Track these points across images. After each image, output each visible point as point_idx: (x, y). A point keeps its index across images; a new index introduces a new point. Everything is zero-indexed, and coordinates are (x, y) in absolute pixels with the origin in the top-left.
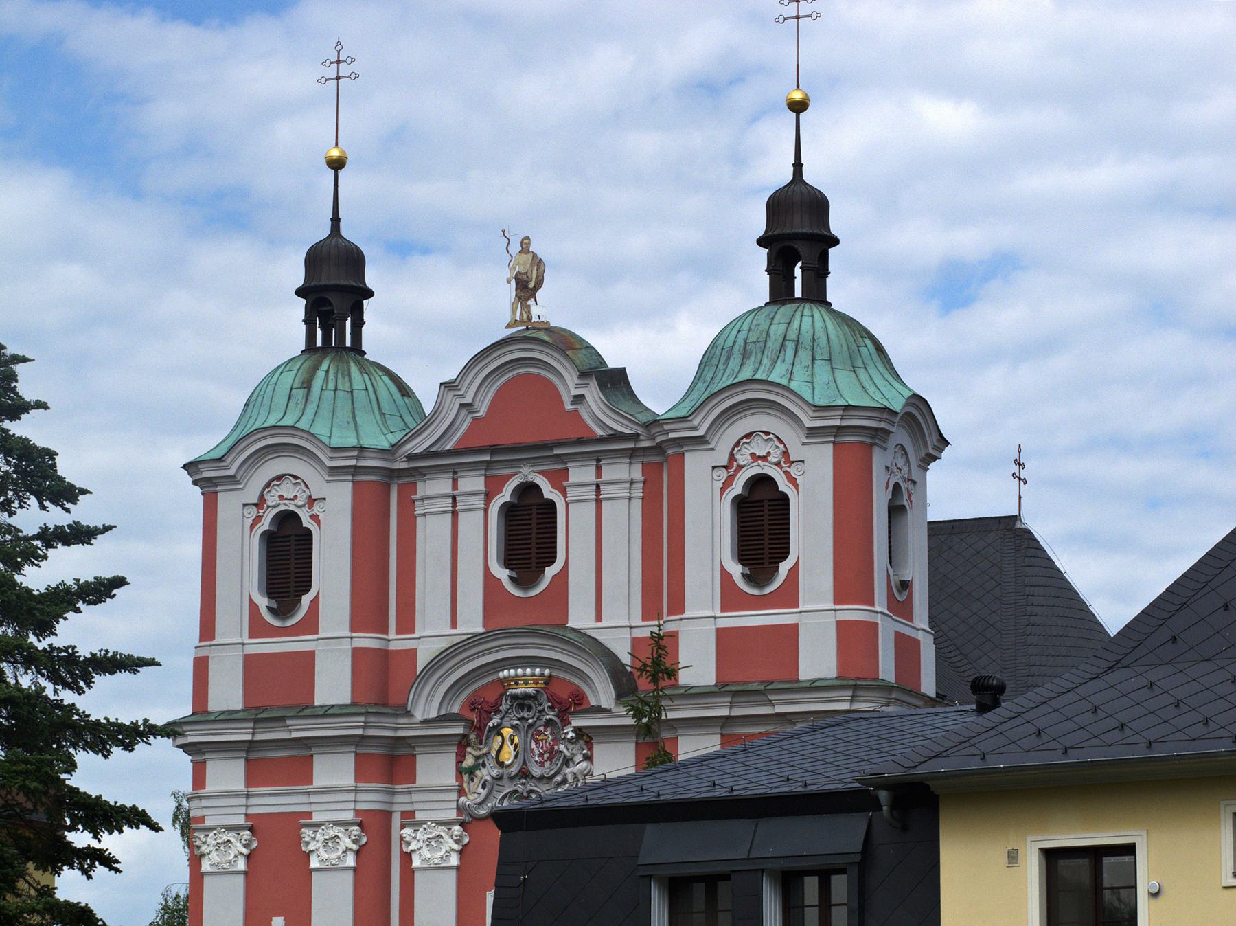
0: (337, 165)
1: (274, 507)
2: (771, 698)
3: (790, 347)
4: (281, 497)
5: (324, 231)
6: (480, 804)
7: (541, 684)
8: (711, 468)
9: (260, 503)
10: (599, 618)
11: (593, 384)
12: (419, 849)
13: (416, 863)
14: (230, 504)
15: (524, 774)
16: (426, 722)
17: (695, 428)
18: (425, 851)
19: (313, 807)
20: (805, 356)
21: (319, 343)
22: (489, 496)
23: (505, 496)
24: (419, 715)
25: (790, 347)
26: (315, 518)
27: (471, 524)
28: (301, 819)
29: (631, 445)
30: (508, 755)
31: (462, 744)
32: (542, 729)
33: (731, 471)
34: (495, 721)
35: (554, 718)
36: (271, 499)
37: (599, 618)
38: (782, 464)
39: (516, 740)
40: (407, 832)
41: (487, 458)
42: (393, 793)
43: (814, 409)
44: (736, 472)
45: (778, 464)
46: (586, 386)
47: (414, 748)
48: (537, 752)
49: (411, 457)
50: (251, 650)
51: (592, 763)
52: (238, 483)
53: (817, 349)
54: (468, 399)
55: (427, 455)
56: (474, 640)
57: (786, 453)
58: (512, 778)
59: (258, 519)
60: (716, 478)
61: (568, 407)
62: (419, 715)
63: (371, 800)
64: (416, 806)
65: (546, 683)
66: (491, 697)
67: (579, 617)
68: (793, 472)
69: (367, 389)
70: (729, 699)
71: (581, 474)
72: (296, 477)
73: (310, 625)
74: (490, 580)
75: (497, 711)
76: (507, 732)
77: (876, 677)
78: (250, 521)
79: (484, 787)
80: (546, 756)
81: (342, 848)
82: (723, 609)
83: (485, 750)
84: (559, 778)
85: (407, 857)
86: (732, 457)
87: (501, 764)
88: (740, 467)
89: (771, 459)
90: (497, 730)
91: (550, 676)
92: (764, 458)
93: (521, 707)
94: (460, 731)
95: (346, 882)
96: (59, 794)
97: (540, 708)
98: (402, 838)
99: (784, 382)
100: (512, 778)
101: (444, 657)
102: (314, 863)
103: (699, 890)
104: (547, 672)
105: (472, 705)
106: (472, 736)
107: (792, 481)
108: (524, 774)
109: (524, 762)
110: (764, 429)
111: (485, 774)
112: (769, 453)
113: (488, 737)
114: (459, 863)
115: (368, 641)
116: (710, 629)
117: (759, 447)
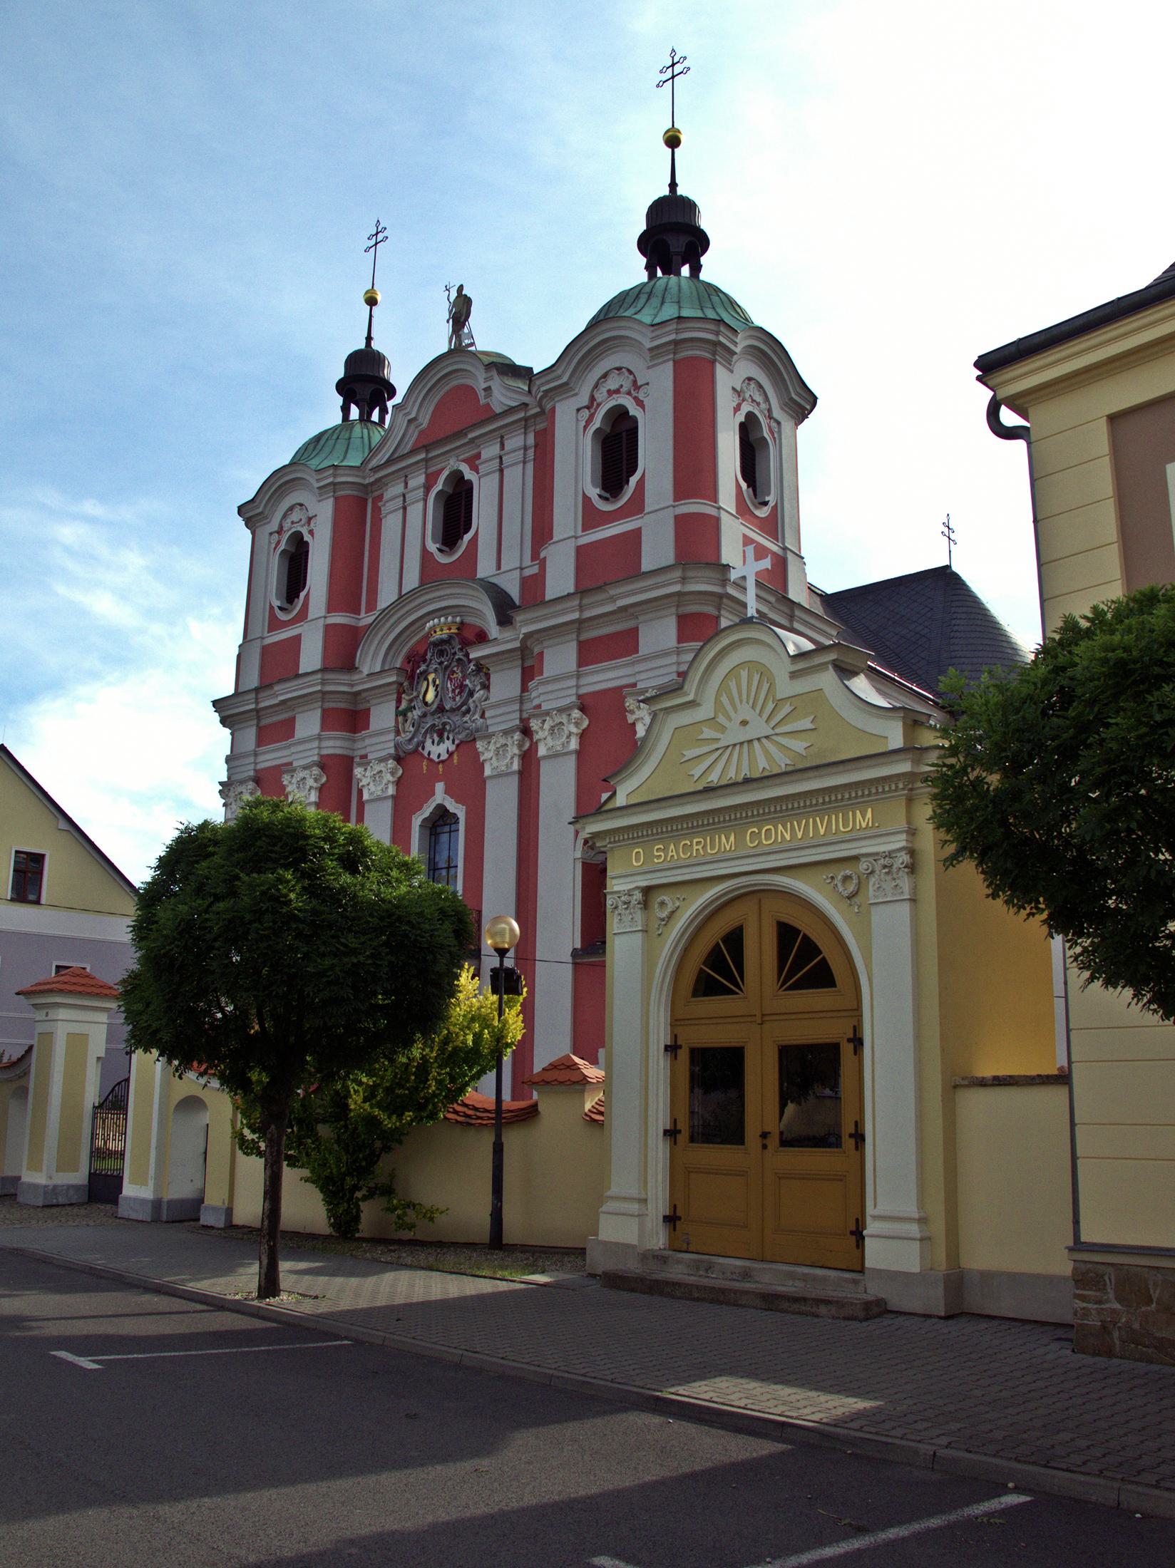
2: (612, 592)
4: (293, 523)
6: (410, 740)
7: (454, 630)
8: (575, 411)
9: (279, 532)
11: (494, 373)
12: (368, 785)
13: (366, 796)
17: (559, 377)
18: (372, 787)
19: (294, 757)
22: (427, 488)
28: (288, 768)
29: (522, 415)
30: (430, 697)
32: (455, 669)
33: (592, 411)
34: (423, 667)
35: (462, 657)
36: (287, 525)
37: (499, 567)
38: (632, 392)
39: (437, 682)
41: (423, 456)
42: (354, 741)
43: (652, 328)
46: (491, 378)
47: (368, 701)
48: (450, 689)
49: (376, 469)
51: (489, 691)
52: (266, 518)
54: (413, 416)
55: (390, 462)
57: (635, 382)
58: (433, 714)
60: (580, 419)
62: (366, 670)
63: (334, 745)
64: (368, 749)
65: (458, 629)
67: (485, 568)
69: (362, 437)
70: (577, 602)
72: (301, 505)
73: (636, 506)
74: (425, 553)
75: (425, 661)
78: (273, 545)
79: (413, 726)
80: (457, 691)
81: (385, 781)
83: (415, 694)
85: (360, 792)
86: (592, 398)
87: (426, 704)
88: (599, 405)
89: (624, 389)
90: (425, 675)
91: (462, 623)
92: (617, 391)
93: (441, 653)
94: (393, 679)
95: (570, 764)
96: (1165, 659)
97: (453, 651)
100: (433, 714)
101: (382, 618)
102: (488, 771)
103: (746, 744)
104: (458, 619)
106: (406, 684)
107: (640, 403)
108: (441, 709)
109: (441, 700)
110: (630, 368)
111: (417, 713)
112: (622, 386)
113: (418, 683)
114: (395, 793)
115: (338, 619)
117: (612, 384)
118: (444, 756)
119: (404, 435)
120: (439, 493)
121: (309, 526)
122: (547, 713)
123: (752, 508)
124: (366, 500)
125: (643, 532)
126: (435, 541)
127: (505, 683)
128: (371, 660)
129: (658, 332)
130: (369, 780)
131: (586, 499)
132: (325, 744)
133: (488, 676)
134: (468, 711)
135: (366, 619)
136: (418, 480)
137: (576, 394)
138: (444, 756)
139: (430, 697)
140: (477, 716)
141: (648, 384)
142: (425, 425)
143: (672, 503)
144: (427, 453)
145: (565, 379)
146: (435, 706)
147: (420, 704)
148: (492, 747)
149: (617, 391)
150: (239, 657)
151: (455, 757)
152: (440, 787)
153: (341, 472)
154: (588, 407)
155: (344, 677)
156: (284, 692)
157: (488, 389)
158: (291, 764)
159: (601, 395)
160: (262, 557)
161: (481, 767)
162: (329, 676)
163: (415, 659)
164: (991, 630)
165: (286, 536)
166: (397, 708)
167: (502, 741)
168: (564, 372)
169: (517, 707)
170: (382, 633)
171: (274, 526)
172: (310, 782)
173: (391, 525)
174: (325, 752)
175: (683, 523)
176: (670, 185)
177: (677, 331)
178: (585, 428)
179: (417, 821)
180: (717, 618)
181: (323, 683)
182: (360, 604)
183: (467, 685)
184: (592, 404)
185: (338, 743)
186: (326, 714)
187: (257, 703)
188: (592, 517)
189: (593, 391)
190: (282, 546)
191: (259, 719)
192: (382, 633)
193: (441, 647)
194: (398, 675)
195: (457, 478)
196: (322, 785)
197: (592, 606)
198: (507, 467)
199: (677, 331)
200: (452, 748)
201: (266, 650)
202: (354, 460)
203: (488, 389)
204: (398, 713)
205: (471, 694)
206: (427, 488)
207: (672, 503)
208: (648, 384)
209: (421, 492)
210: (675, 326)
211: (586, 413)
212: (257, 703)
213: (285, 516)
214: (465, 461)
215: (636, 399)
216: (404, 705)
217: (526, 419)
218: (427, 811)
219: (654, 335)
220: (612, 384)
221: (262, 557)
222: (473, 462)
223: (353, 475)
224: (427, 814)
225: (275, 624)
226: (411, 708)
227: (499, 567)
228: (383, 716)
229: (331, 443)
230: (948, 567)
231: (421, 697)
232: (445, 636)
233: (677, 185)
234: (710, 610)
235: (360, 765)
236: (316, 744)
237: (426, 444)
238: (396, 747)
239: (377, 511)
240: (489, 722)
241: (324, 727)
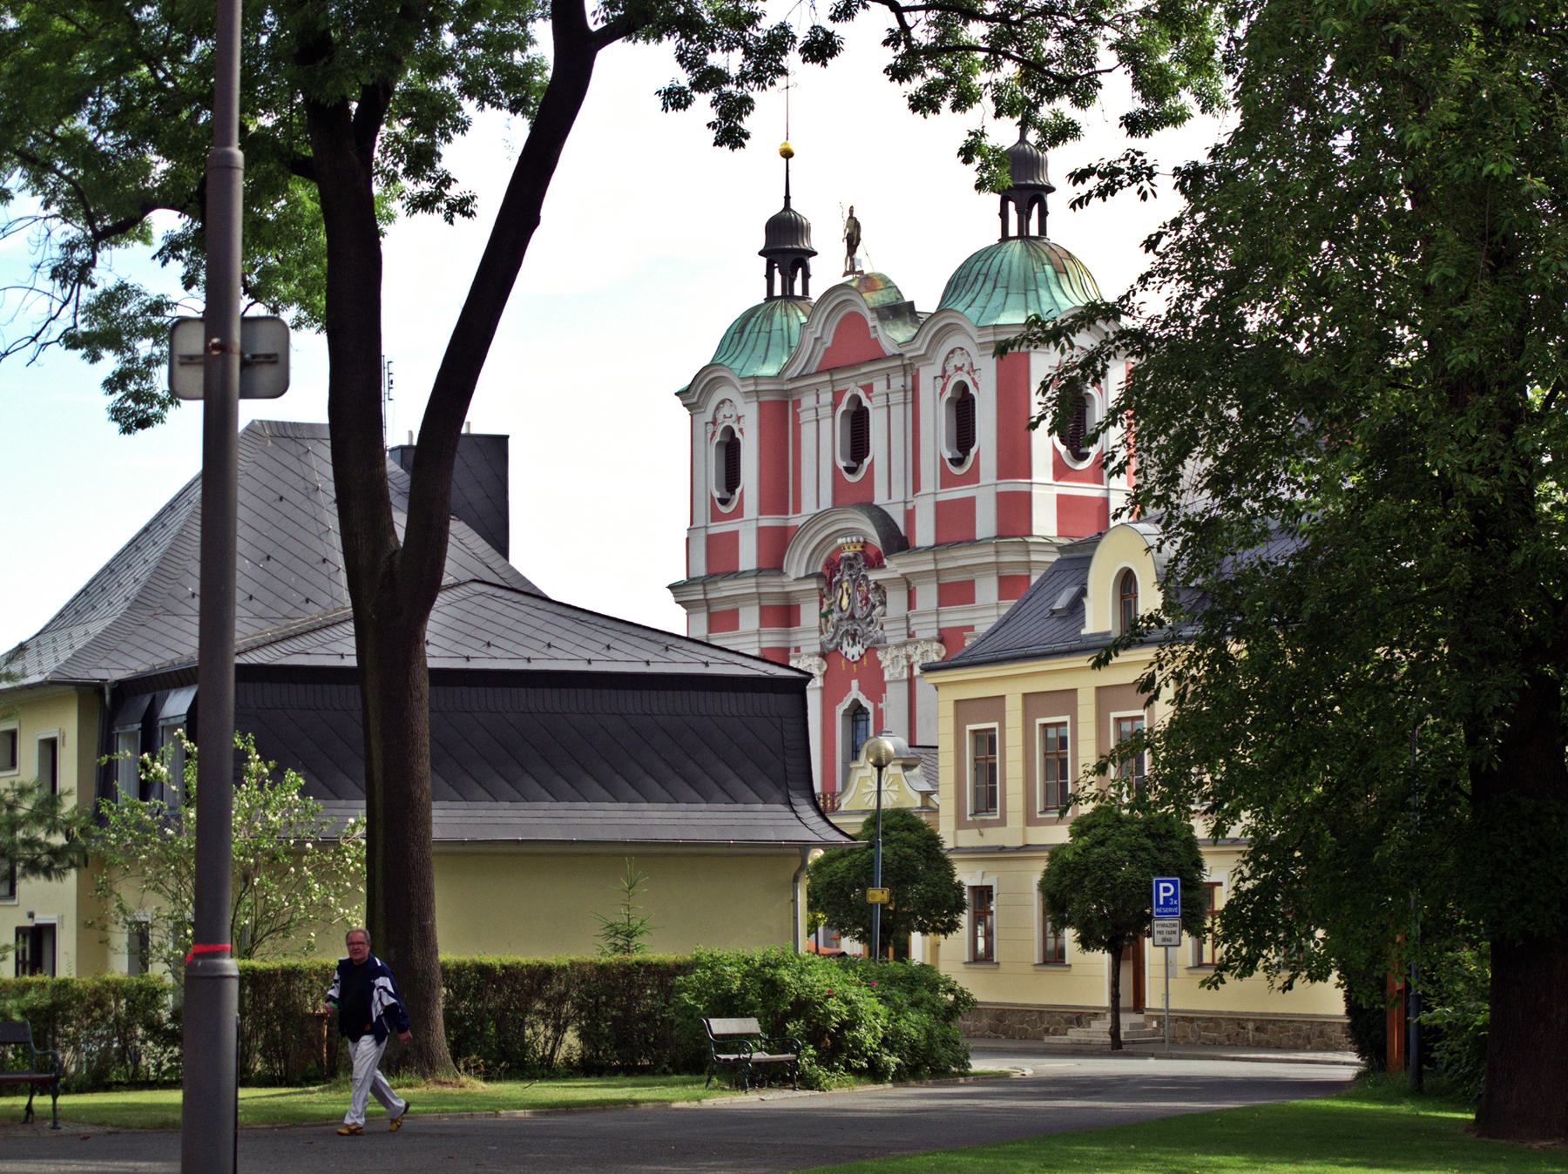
0: (787, 154)
3: (981, 278)
5: (779, 206)
6: (832, 640)
7: (859, 549)
9: (714, 422)
15: (852, 616)
16: (798, 579)
17: (919, 349)
20: (989, 285)
21: (778, 291)
22: (835, 406)
24: (793, 576)
25: (981, 278)
27: (826, 425)
36: (720, 418)
37: (890, 498)
49: (792, 380)
50: (941, 498)
52: (700, 407)
53: (1000, 280)
54: (818, 335)
55: (800, 377)
56: (825, 514)
59: (714, 434)
72: (962, 349)
77: (734, 569)
82: (942, 487)
86: (944, 370)
90: (840, 582)
94: (814, 586)
102: (887, 678)
108: (852, 616)
115: (769, 521)
116: (754, 525)
118: (857, 658)
120: (844, 412)
122: (918, 642)
123: (1070, 464)
124: (786, 403)
125: (978, 502)
126: (843, 458)
127: (896, 602)
128: (796, 565)
132: (764, 638)
133: (884, 593)
134: (872, 621)
135: (796, 520)
136: (827, 397)
138: (857, 658)
139: (845, 602)
140: (878, 628)
142: (829, 344)
144: (831, 375)
145: (922, 352)
146: (848, 613)
148: (889, 657)
149: (960, 369)
150: (688, 540)
151: (865, 660)
152: (855, 683)
153: (760, 381)
154: (942, 377)
155: (776, 580)
156: (726, 589)
160: (699, 456)
161: (882, 673)
162: (762, 580)
163: (832, 566)
165: (720, 428)
167: (895, 653)
169: (904, 625)
170: (804, 541)
173: (808, 432)
174: (765, 645)
175: (1002, 498)
179: (840, 709)
180: (1029, 577)
181: (758, 585)
182: (787, 505)
184: (944, 375)
185: (770, 638)
186: (764, 611)
187: (705, 594)
188: (947, 480)
190: (717, 438)
191: (709, 607)
192: (804, 541)
193: (850, 563)
195: (856, 400)
197: (943, 560)
199: (995, 334)
200: (862, 652)
201: (710, 539)
202: (770, 370)
205: (874, 607)
206: (835, 406)
207: (994, 480)
209: (829, 409)
211: (940, 382)
212: (705, 594)
213: (717, 408)
214: (862, 387)
216: (825, 609)
218: (845, 704)
221: (699, 456)
224: (846, 706)
225: (716, 516)
226: (830, 611)
227: (890, 498)
228: (810, 614)
229: (754, 336)
232: (851, 554)
234: (1022, 572)
235: (795, 657)
237: (828, 368)
238: (822, 644)
239: (796, 416)
240: (887, 634)
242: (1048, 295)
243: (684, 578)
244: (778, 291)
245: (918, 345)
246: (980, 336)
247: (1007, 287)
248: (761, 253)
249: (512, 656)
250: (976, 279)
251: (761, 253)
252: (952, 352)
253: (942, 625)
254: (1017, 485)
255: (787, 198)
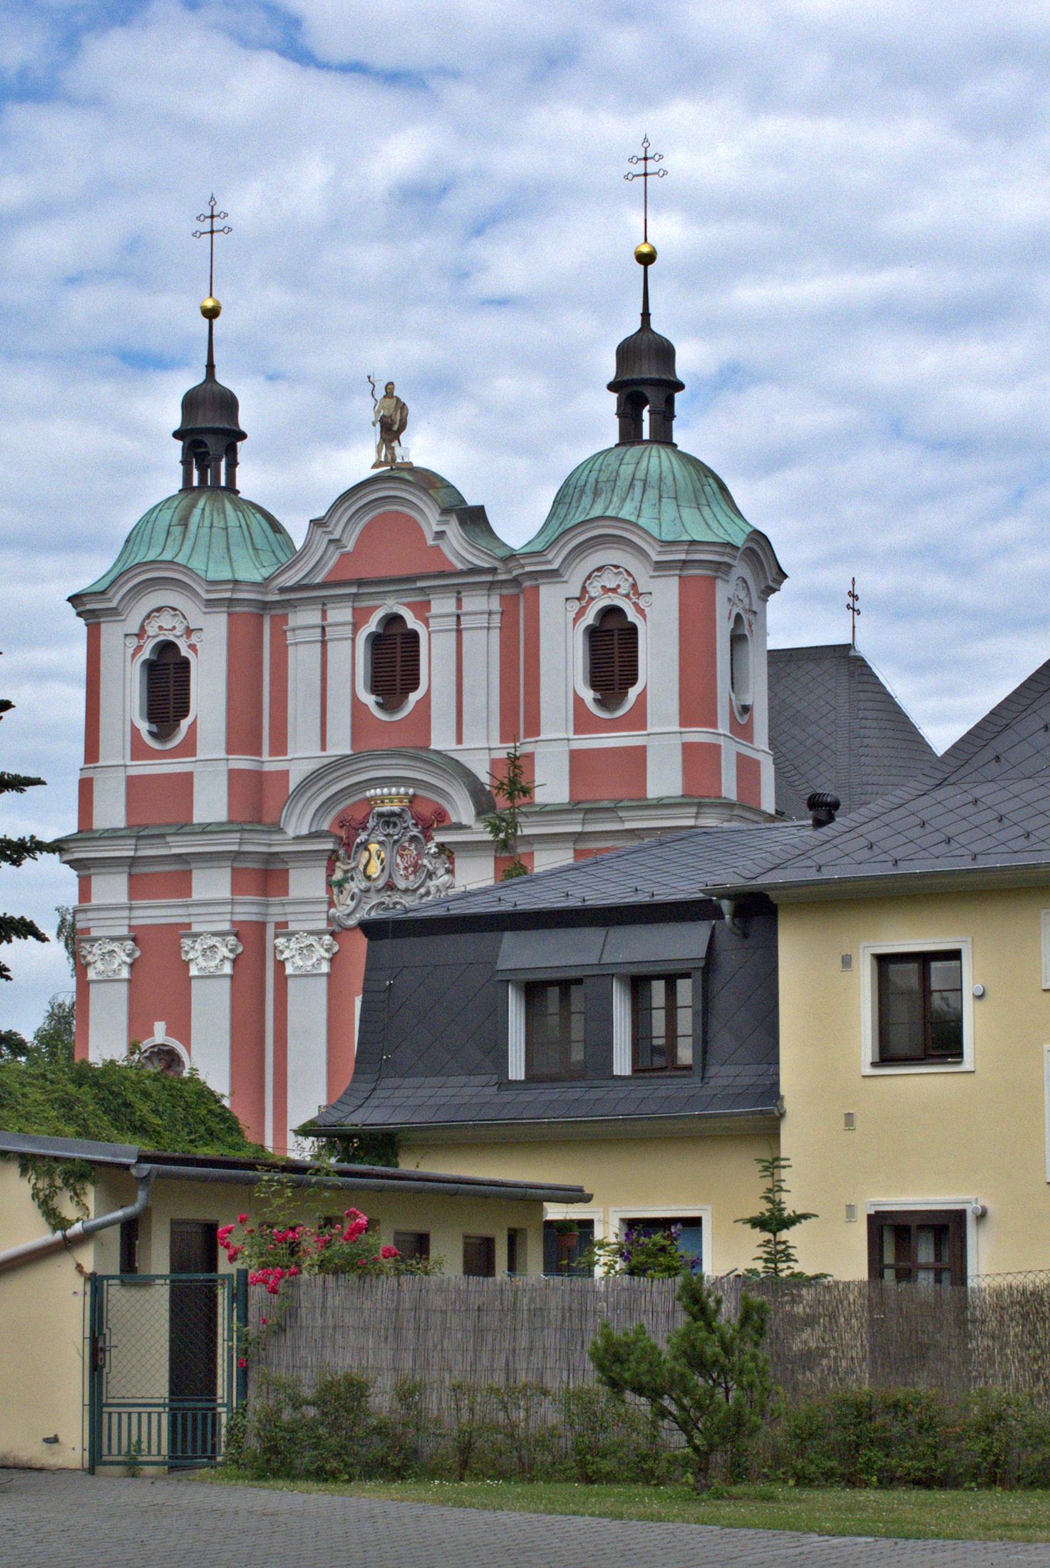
1: (155, 637)
4: (161, 628)
9: (141, 634)
10: (459, 740)
13: (289, 970)
14: (112, 634)
16: (297, 838)
17: (549, 562)
19: (193, 919)
21: (195, 483)
22: (356, 627)
23: (372, 626)
24: (291, 833)
25: (638, 485)
26: (193, 647)
29: (489, 578)
30: (375, 869)
31: (332, 859)
33: (584, 603)
34: (362, 837)
36: (152, 630)
37: (459, 740)
39: (383, 855)
40: (281, 941)
41: (354, 590)
42: (267, 905)
44: (588, 603)
45: (627, 596)
47: (287, 862)
49: (283, 590)
51: (454, 876)
52: (119, 614)
57: (634, 586)
61: (430, 542)
62: (291, 833)
66: (359, 816)
67: (441, 740)
68: (642, 603)
71: (442, 605)
73: (188, 748)
74: (357, 705)
75: (365, 828)
76: (374, 847)
80: (410, 870)
83: (353, 865)
84: (422, 891)
85: (280, 965)
87: (369, 878)
88: (592, 599)
89: (622, 591)
90: (364, 846)
92: (614, 590)
94: (330, 846)
97: (405, 825)
98: (275, 947)
99: (633, 519)
102: (194, 971)
105: (342, 822)
106: (341, 852)
107: (641, 611)
108: (390, 887)
109: (390, 876)
111: (353, 887)
112: (619, 586)
113: (356, 852)
115: (243, 762)
117: (609, 580)
119: (322, 557)
121: (188, 638)
125: (649, 754)
129: (667, 549)
130: (294, 952)
131: (578, 701)
132: (238, 909)
137: (566, 582)
141: (650, 593)
143: (677, 728)
147: (361, 877)
157: (440, 535)
158: (189, 925)
159: (594, 590)
161: (186, 964)
164: (880, 715)
166: (329, 876)
168: (556, 556)
171: (133, 625)
172: (224, 951)
173: (302, 661)
176: (642, 315)
177: (687, 553)
178: (575, 620)
183: (425, 866)
185: (254, 909)
189: (585, 582)
194: (334, 843)
196: (238, 955)
198: (332, 640)
203: (440, 535)
204: (330, 885)
208: (650, 593)
209: (348, 631)
210: (686, 547)
215: (635, 604)
217: (492, 583)
219: (663, 549)
220: (609, 580)
222: (422, 609)
223: (254, 592)
230: (849, 647)
231: (361, 868)
233: (649, 315)
236: (228, 908)
241: (236, 888)
242: (710, 512)
243: (566, 800)
244: (195, 483)
245: (550, 557)
246: (660, 553)
247: (676, 498)
248: (176, 435)
249: (989, 851)
250: (631, 486)
251: (176, 435)
252: (159, 610)
253: (135, 922)
254: (698, 735)
255: (646, 315)
